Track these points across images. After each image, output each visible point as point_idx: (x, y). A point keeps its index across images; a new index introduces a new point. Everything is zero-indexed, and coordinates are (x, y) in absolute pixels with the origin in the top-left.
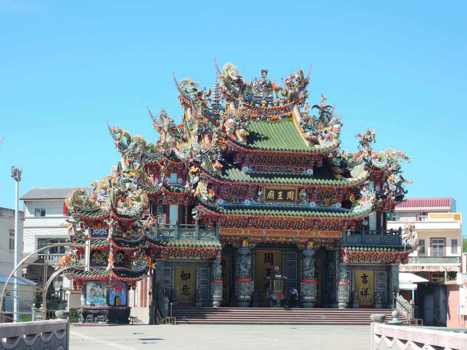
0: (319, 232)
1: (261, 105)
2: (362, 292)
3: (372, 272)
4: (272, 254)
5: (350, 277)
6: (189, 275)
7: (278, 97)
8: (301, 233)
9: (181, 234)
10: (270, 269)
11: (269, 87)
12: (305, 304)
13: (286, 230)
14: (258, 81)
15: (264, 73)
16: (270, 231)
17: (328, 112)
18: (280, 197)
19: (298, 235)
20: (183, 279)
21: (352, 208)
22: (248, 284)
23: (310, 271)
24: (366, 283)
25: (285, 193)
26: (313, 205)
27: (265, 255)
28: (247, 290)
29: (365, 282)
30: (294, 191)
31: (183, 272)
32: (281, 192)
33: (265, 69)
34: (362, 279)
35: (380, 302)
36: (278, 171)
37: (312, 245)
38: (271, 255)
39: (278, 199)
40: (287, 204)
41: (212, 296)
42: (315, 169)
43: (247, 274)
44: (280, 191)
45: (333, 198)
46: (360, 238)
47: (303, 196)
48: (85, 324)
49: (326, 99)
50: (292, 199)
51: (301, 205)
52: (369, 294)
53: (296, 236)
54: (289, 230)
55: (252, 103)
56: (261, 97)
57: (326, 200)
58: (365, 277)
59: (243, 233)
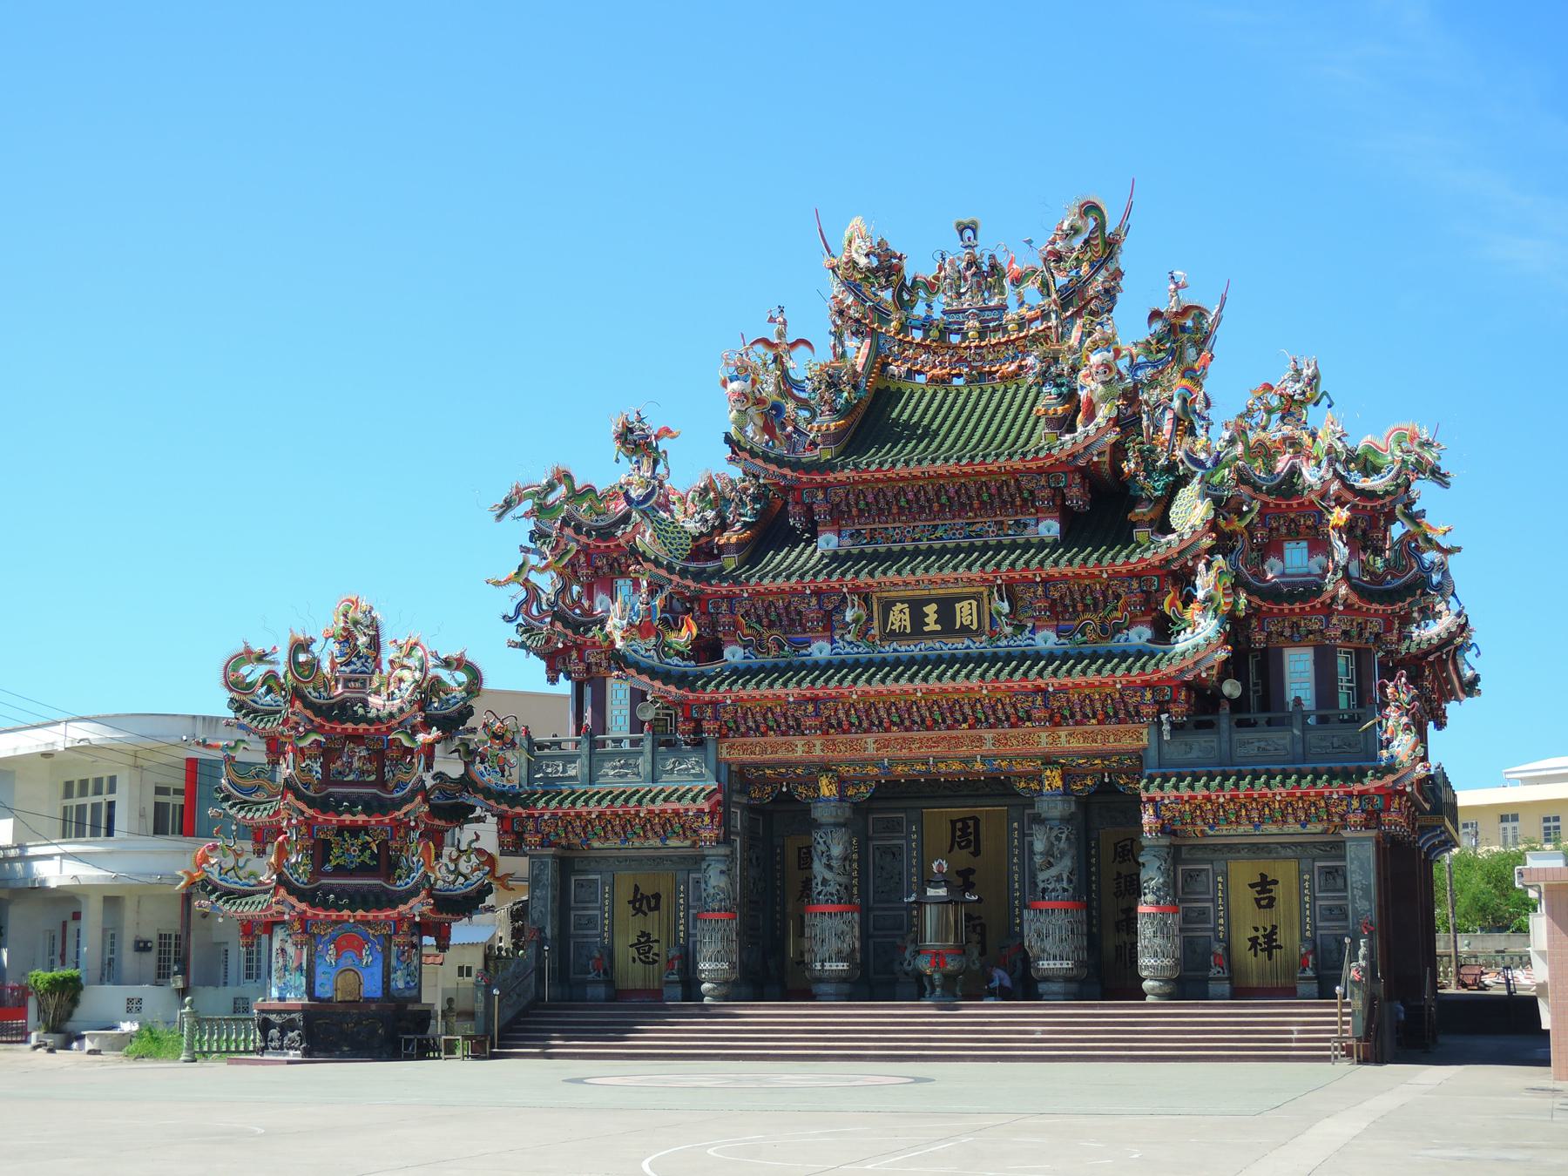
1: (965, 336)
2: (1254, 940)
3: (1293, 865)
4: (976, 821)
5: (1180, 890)
6: (657, 897)
7: (1022, 304)
8: (997, 741)
9: (602, 767)
10: (971, 871)
11: (989, 275)
12: (1042, 987)
13: (944, 733)
14: (952, 263)
15: (968, 233)
16: (888, 740)
18: (931, 624)
19: (988, 747)
20: (638, 911)
21: (1173, 640)
22: (837, 924)
23: (1053, 872)
25: (946, 608)
26: (1046, 640)
27: (953, 823)
28: (833, 945)
29: (1263, 903)
30: (977, 597)
31: (637, 888)
32: (934, 607)
33: (966, 220)
34: (1253, 893)
35: (1309, 973)
36: (941, 538)
37: (1058, 783)
38: (971, 823)
39: (926, 629)
40: (960, 645)
41: (695, 964)
42: (1069, 519)
43: (832, 889)
44: (928, 602)
46: (1215, 744)
47: (999, 614)
48: (266, 1057)
49: (1184, 286)
50: (974, 627)
51: (1005, 643)
52: (1280, 947)
53: (981, 749)
54: (954, 733)
55: (934, 333)
56: (964, 311)
57: (1092, 620)
58: (1264, 885)
59: (800, 753)
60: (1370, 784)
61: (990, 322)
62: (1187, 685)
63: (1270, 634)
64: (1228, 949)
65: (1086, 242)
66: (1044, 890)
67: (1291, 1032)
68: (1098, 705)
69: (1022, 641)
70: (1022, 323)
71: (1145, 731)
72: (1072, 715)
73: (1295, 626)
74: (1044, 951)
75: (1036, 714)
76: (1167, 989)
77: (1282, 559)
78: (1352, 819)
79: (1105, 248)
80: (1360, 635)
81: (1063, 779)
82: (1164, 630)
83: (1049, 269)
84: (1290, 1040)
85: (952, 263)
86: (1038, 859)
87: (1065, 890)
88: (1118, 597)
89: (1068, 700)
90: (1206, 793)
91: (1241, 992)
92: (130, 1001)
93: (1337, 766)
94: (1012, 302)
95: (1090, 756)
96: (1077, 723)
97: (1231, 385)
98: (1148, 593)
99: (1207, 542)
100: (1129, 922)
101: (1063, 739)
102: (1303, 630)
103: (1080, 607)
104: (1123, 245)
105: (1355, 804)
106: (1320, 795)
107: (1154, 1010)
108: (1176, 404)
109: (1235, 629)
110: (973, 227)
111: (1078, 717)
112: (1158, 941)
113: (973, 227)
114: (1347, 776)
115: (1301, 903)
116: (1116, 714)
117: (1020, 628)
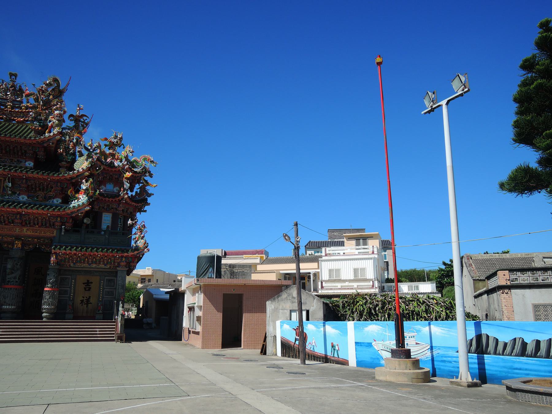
0: (25, 229)
2: (82, 301)
5: (60, 284)
15: (14, 77)
17: (84, 122)
23: (13, 275)
24: (89, 290)
26: (23, 198)
33: (14, 73)
35: (101, 312)
37: (20, 246)
45: (51, 191)
47: (7, 187)
49: (82, 109)
52: (91, 303)
57: (41, 194)
58: (88, 284)
60: (130, 253)
61: (16, 104)
62: (72, 217)
63: (100, 207)
64: (73, 303)
65: (53, 89)
66: (8, 282)
67: (96, 331)
68: (40, 220)
69: (14, 198)
70: (27, 108)
71: (55, 231)
72: (29, 223)
73: (108, 206)
74: (5, 302)
75: (16, 221)
76: (51, 316)
77: (105, 186)
78: (122, 264)
79: (59, 93)
80: (127, 211)
81: (22, 245)
82: (67, 200)
83: (39, 94)
84: (97, 334)
85: (6, 85)
86: (8, 271)
87: (16, 282)
88: (52, 188)
89: (29, 218)
90: (75, 252)
91: (77, 317)
92: (536, 307)
93: (118, 248)
94: (25, 100)
95: (33, 237)
96: (30, 226)
97: (93, 137)
98: (63, 188)
99: (87, 174)
100: (39, 295)
101: (25, 231)
102: (110, 207)
103: (37, 189)
104: (65, 94)
105: (124, 259)
106: (113, 256)
107: (45, 324)
108: (75, 141)
109: (91, 202)
110: (16, 75)
111: (32, 224)
112: (50, 300)
113: (16, 75)
114: (123, 251)
115: (100, 290)
116: (46, 224)
117: (14, 193)
